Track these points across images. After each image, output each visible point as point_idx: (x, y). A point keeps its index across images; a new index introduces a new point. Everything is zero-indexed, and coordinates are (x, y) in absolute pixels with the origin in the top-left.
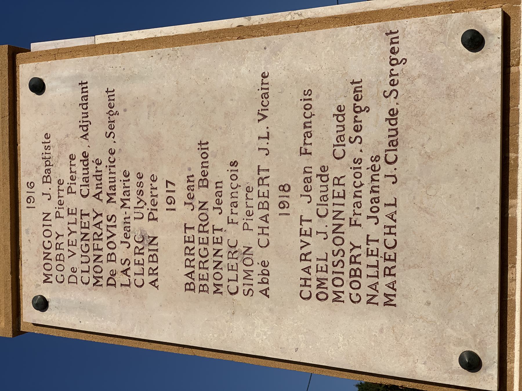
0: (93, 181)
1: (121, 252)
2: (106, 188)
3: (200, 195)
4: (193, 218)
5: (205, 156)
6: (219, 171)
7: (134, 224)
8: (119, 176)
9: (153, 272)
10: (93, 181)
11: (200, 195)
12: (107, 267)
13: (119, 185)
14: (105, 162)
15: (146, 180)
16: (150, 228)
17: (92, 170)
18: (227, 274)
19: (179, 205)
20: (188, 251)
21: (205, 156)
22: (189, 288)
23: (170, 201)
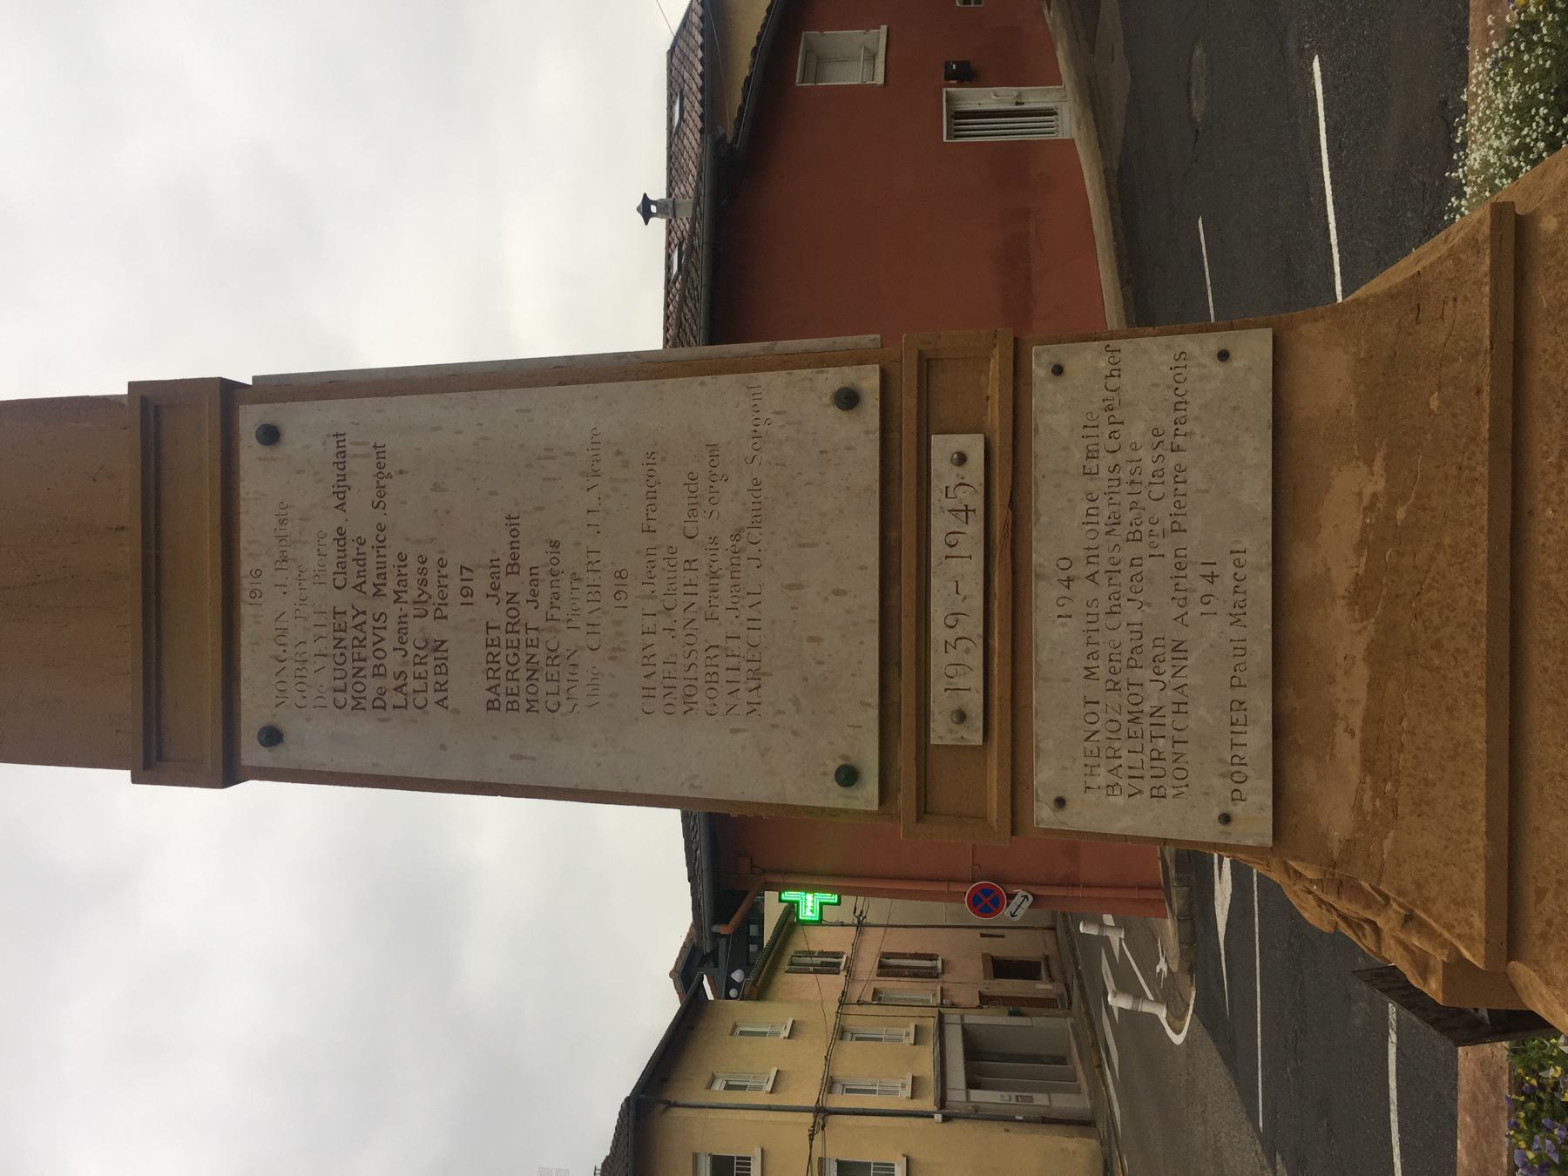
0: (353, 568)
1: (393, 662)
2: (372, 577)
5: (514, 533)
6: (533, 555)
7: (414, 626)
8: (392, 560)
9: (441, 687)
10: (353, 568)
11: (508, 585)
12: (372, 686)
14: (371, 541)
15: (432, 563)
16: (435, 630)
17: (351, 551)
20: (492, 659)
21: (514, 533)
22: (491, 706)
23: (467, 593)
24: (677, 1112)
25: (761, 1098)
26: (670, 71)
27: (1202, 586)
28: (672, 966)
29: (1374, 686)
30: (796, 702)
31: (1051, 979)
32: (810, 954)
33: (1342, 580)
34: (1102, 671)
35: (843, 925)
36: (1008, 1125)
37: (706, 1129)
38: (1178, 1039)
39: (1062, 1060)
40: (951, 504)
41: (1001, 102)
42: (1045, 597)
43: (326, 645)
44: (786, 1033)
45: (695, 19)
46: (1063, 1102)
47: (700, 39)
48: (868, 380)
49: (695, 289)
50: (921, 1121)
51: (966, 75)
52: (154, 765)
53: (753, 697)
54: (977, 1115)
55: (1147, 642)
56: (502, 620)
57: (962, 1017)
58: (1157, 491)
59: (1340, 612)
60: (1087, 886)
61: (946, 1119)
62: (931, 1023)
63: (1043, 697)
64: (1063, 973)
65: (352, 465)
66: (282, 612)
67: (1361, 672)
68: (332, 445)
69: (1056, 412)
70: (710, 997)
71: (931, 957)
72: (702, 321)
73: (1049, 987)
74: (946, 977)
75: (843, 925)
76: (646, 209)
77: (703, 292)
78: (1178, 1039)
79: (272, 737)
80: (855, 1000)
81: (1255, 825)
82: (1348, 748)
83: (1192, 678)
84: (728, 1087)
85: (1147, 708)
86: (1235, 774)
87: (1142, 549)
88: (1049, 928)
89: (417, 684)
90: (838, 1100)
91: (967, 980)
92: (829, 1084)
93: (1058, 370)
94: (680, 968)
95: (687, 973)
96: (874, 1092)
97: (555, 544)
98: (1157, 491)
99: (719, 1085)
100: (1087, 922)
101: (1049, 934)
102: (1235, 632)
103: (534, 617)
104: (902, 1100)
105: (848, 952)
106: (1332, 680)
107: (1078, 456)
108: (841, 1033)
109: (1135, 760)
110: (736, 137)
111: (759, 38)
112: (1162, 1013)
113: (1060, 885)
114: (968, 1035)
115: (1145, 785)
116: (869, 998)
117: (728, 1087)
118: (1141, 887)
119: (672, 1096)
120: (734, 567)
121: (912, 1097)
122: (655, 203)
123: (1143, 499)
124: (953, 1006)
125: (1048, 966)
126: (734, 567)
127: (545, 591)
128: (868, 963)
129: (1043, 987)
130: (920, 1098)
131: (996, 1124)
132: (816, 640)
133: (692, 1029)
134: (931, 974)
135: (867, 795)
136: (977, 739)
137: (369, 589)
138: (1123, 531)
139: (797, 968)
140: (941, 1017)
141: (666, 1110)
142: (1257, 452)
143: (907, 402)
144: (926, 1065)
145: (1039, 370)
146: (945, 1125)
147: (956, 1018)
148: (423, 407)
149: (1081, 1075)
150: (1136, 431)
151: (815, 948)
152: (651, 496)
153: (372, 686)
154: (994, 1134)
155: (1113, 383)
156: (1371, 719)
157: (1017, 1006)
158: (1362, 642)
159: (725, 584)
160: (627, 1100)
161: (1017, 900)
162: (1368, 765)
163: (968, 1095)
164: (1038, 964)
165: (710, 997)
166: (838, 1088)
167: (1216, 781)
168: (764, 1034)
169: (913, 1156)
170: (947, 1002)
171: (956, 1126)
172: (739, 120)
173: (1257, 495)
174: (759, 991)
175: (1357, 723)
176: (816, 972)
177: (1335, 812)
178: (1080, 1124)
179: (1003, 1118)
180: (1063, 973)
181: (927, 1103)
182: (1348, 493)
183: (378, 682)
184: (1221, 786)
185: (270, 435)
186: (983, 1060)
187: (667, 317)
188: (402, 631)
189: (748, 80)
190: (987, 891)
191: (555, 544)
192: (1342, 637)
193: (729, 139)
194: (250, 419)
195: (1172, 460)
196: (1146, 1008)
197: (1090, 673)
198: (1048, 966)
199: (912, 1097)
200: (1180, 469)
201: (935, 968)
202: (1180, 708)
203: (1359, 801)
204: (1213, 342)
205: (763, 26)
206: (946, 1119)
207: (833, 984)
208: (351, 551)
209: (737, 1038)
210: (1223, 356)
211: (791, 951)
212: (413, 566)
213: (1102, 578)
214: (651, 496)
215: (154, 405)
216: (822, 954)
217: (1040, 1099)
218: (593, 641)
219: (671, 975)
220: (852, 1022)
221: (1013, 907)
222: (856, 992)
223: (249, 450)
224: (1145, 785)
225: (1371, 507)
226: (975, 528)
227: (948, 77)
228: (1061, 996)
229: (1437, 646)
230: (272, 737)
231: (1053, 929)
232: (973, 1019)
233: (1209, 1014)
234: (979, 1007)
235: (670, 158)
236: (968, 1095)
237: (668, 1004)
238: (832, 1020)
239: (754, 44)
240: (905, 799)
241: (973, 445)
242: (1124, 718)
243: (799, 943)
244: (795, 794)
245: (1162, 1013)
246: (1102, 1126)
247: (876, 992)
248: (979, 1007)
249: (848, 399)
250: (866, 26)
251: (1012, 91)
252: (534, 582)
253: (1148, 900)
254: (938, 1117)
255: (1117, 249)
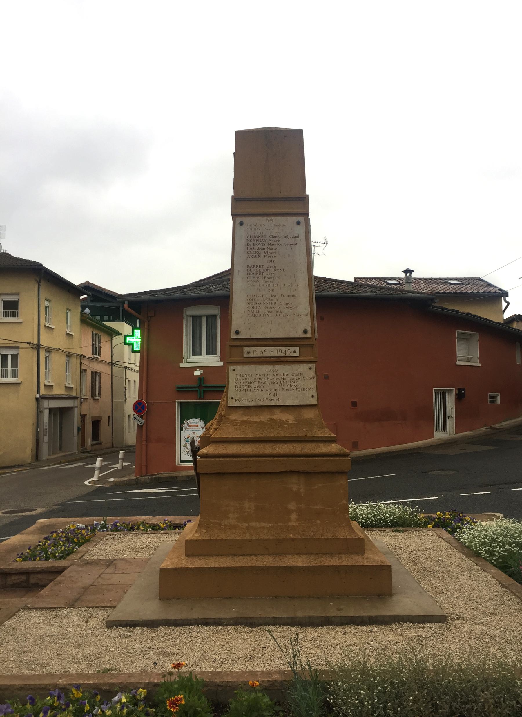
0: (274, 239)
1: (256, 247)
2: (272, 243)
3: (271, 269)
4: (265, 267)
5: (280, 270)
6: (277, 274)
7: (263, 251)
8: (275, 247)
9: (251, 256)
10: (274, 239)
11: (271, 269)
12: (252, 243)
13: (273, 247)
14: (279, 243)
15: (275, 254)
16: (262, 255)
17: (276, 239)
18: (252, 276)
19: (268, 263)
20: (257, 266)
21: (280, 270)
22: (248, 266)
23: (269, 261)
24: (36, 286)
25: (43, 322)
26: (472, 279)
27: (273, 394)
28: (91, 282)
29: (256, 422)
30: (250, 323)
31: (92, 445)
32: (100, 342)
33: (274, 417)
34: (257, 377)
35: (112, 356)
36: (35, 425)
37: (29, 298)
38: (86, 483)
39: (60, 449)
40: (287, 350)
41: (449, 410)
42: (270, 367)
43: (259, 234)
44: (68, 332)
45: (490, 289)
46: (45, 448)
47: (481, 291)
48: (309, 335)
49: (376, 292)
50: (36, 389)
51: (460, 397)
52: (236, 200)
53: (251, 315)
54: (39, 412)
55: (263, 385)
56: (264, 268)
57: (77, 407)
58: (289, 386)
59: (269, 417)
60: (147, 446)
61: (37, 399)
62: (74, 394)
63: (253, 367)
64: (95, 451)
65: (293, 239)
66: (266, 226)
67: (258, 420)
68: (297, 235)
69: (303, 368)
70: (81, 297)
71: (100, 394)
72: (363, 295)
73: (89, 444)
74: (92, 400)
75: (112, 356)
76: (408, 271)
77: (374, 295)
78: (86, 483)
79: (241, 224)
80: (82, 361)
81: (231, 403)
82: (245, 418)
83: (256, 392)
84: (46, 307)
85: (251, 385)
86: (240, 400)
87: (279, 383)
88: (113, 445)
89: (252, 252)
90: (43, 354)
91: (92, 410)
92: (49, 350)
93: (310, 369)
94: (90, 285)
95: (88, 288)
96: (46, 369)
97: (279, 278)
98: (289, 386)
99: (47, 303)
100: (125, 454)
101: (110, 445)
102: (265, 399)
103: (265, 274)
104: (44, 381)
105: (101, 359)
106: (257, 416)
107: (295, 372)
108: (69, 355)
109: (242, 383)
110: (435, 307)
111: (475, 316)
112: (94, 479)
113: (147, 436)
114: (70, 409)
115: (238, 385)
116: (83, 367)
117: (46, 307)
118: (147, 467)
119: (42, 284)
120: (275, 311)
121: (45, 385)
122: (410, 275)
123: (288, 383)
124: (81, 403)
125: (97, 444)
126: (275, 311)
127: (270, 276)
128: (97, 367)
129: (89, 441)
130: (45, 388)
131: (35, 420)
132: (262, 326)
133: (69, 292)
134: (93, 394)
135: (234, 336)
136: (245, 356)
137: (270, 242)
138: (282, 380)
139: (94, 337)
140: (77, 398)
141: (37, 281)
142: (296, 402)
143: (305, 342)
144: (58, 391)
145: (310, 366)
146: (34, 400)
147: (76, 405)
148: (303, 258)
149: (55, 456)
150: (300, 382)
151: (102, 345)
152: (288, 296)
153: (252, 243)
154: (31, 420)
155: (308, 378)
156: (250, 422)
157: (81, 430)
158: (264, 420)
159: (272, 310)
160: (41, 265)
161: (141, 420)
162: (242, 421)
163: (46, 408)
164: (98, 441)
165: (81, 297)
166: (47, 354)
167: (239, 396)
168: (67, 323)
169: (21, 386)
170: (82, 400)
171: (34, 404)
172: (441, 308)
173: (289, 402)
174: (84, 321)
175: (249, 420)
176: (93, 345)
177: (234, 416)
178: (37, 456)
179: (38, 423)
180: (95, 451)
181: (43, 392)
182: (289, 418)
183: (252, 245)
184: (238, 398)
185: (298, 223)
186: (60, 414)
187: (370, 278)
188: (262, 249)
189: (458, 311)
190: (143, 407)
191: (279, 278)
192: (264, 417)
193: (435, 304)
194: (302, 219)
195: (295, 388)
196: (96, 472)
197: (257, 375)
198: (97, 444)
199: (45, 385)
200: (293, 390)
201: (95, 396)
202: (251, 390)
203: (236, 420)
204: (315, 395)
205: (480, 317)
206: (37, 399)
207: (88, 352)
208: (276, 239)
209: (66, 311)
210: (313, 396)
211: (101, 334)
212: (274, 251)
213: (274, 377)
214: (288, 296)
215: (304, 200)
216: (100, 348)
217: (46, 439)
218: (261, 285)
219: (87, 282)
220: (73, 360)
221: (138, 418)
222: (85, 362)
223: (296, 219)
224: (238, 385)
225: (287, 421)
226: (282, 355)
227: (459, 390)
228: (86, 449)
229: (263, 431)
230: (241, 224)
231: (113, 446)
232: (76, 410)
233: (98, 492)
234: (81, 414)
235: (436, 279)
236: (46, 408)
237: (76, 280)
238: (74, 351)
239: (473, 313)
240: (233, 343)
241: (297, 354)
242: (249, 381)
243: (104, 338)
244: (233, 323)
245: (94, 479)
246: (37, 463)
247: (85, 370)
248: (81, 414)
249: (305, 332)
250: (481, 358)
251: (453, 415)
252: (271, 274)
253: (142, 468)
254: (38, 396)
255: (390, 452)
